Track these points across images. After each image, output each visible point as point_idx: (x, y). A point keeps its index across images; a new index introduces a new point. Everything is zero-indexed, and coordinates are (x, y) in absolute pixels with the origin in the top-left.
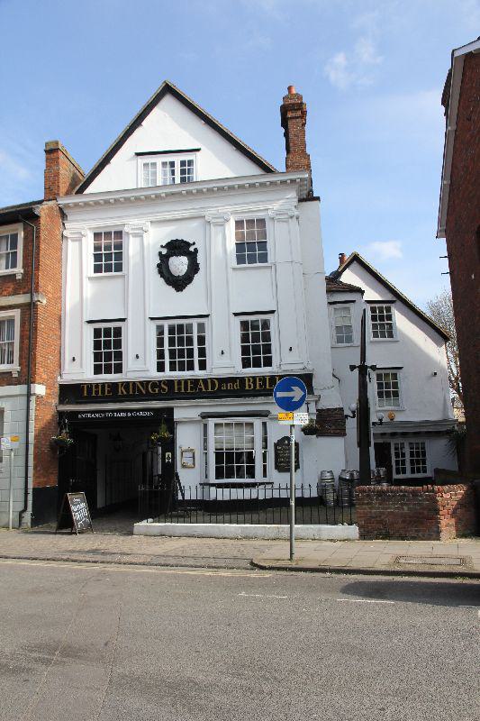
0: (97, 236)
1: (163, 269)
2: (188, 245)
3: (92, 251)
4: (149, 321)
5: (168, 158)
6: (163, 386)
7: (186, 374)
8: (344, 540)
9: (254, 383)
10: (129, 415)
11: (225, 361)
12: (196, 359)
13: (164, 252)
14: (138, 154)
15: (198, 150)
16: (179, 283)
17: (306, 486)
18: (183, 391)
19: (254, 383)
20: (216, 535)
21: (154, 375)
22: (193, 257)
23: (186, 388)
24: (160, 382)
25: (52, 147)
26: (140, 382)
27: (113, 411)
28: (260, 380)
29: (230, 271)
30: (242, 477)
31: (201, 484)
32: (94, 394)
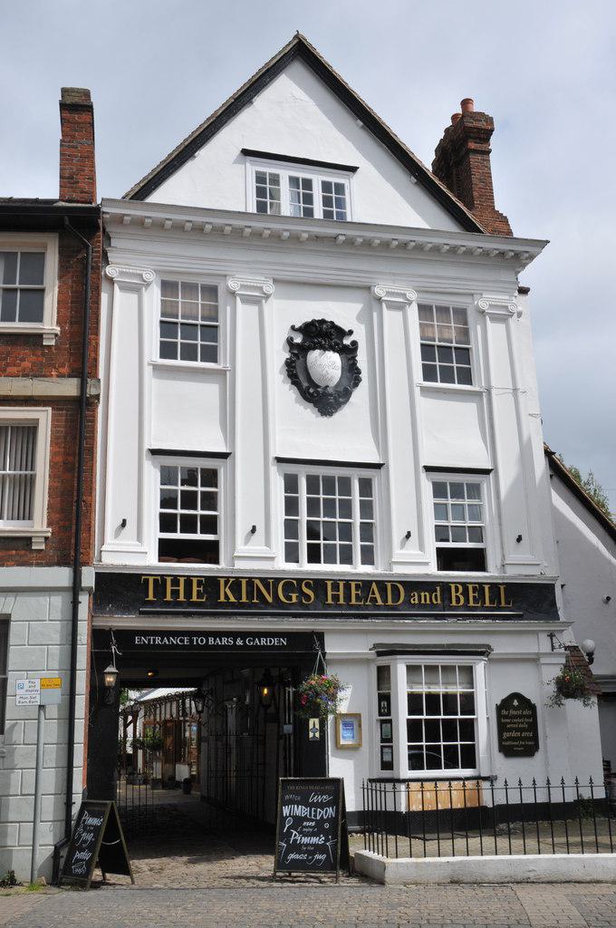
0: (168, 287)
1: (297, 372)
2: (342, 333)
3: (157, 317)
4: (423, 475)
5: (302, 173)
6: (305, 590)
7: (338, 568)
8: (548, 882)
9: (466, 593)
10: (211, 641)
11: (256, 547)
12: (357, 544)
13: (298, 339)
14: (246, 153)
15: (353, 169)
16: (324, 400)
17: (555, 782)
18: (182, 598)
19: (466, 593)
20: (575, 877)
21: (281, 565)
22: (349, 352)
23: (348, 597)
24: (300, 581)
25: (76, 100)
26: (260, 579)
27: (207, 634)
28: (357, 587)
29: (148, 370)
30: (455, 766)
31: (371, 781)
32: (169, 598)
